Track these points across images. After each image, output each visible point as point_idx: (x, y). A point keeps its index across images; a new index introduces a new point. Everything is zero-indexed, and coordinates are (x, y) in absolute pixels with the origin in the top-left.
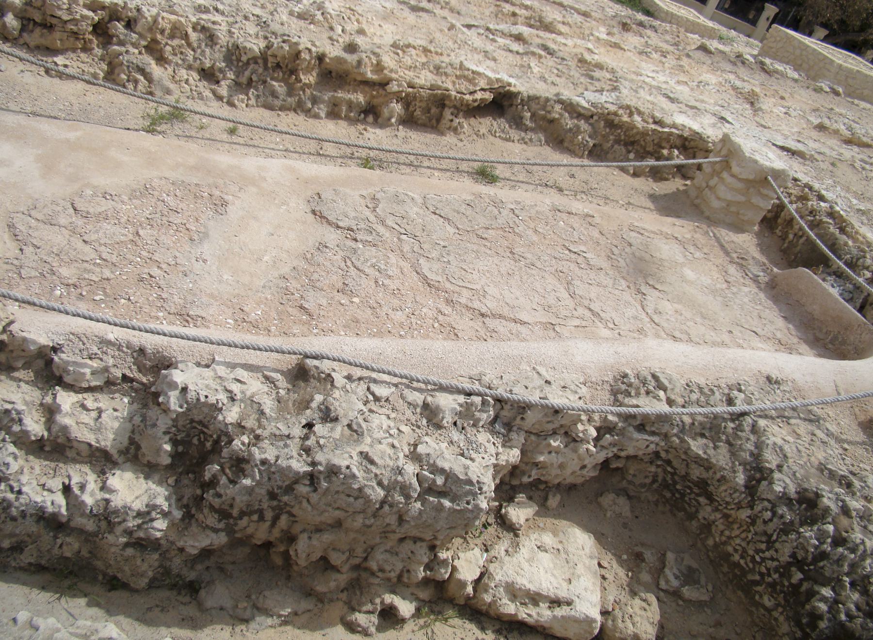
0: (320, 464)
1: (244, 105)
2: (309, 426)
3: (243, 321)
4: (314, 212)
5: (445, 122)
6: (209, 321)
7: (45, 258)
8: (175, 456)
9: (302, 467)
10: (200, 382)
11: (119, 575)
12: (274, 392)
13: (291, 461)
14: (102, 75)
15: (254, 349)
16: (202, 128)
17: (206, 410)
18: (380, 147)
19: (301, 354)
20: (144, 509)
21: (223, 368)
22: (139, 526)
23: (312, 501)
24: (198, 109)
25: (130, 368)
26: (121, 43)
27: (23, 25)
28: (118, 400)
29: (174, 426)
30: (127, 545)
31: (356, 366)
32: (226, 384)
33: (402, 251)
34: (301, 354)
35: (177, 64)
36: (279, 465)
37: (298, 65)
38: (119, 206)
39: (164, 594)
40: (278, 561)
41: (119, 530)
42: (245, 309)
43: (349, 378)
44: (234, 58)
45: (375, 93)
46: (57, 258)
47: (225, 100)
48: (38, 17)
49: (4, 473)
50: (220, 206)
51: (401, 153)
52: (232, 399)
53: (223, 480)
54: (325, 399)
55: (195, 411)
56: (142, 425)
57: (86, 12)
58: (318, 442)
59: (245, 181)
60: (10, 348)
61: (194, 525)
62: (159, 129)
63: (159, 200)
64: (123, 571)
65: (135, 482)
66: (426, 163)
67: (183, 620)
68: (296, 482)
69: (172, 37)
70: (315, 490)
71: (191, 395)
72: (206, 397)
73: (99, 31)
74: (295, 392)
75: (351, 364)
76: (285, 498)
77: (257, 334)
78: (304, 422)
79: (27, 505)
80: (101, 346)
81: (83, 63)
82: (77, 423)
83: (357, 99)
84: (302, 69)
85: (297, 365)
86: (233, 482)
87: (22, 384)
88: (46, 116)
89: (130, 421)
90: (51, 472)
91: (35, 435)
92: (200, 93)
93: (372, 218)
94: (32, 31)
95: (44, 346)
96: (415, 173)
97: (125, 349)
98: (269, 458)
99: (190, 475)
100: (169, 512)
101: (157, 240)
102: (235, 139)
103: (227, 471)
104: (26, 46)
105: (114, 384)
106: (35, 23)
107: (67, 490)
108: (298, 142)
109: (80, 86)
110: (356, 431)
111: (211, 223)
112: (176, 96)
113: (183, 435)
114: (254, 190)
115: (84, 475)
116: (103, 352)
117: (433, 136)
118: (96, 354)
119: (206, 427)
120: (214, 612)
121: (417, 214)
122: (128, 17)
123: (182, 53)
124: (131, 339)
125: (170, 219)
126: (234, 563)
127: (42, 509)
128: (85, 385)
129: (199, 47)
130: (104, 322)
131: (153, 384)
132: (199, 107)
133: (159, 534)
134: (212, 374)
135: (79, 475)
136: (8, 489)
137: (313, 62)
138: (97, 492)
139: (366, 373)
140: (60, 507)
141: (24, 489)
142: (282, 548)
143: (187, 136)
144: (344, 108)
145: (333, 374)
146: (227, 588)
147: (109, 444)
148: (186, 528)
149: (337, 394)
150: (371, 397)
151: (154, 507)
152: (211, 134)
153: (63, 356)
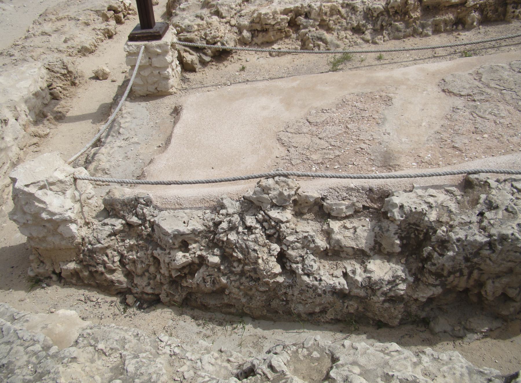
0: (494, 235)
1: (382, 41)
2: (481, 214)
3: (421, 162)
4: (444, 91)
5: (509, 15)
6: (403, 166)
7: (302, 152)
8: (402, 246)
9: (483, 239)
10: (409, 201)
11: (382, 319)
12: (454, 198)
13: (475, 236)
14: (299, 48)
15: (437, 175)
16: (362, 61)
17: (416, 216)
18: (471, 42)
19: (465, 173)
20: (391, 279)
21: (420, 190)
22: (390, 290)
23: (493, 259)
24: (355, 50)
25: (366, 201)
26: (305, 27)
27: (252, 34)
28: (363, 220)
29: (399, 229)
30: (384, 301)
31: (501, 173)
32: (424, 199)
33: (505, 100)
34: (465, 173)
35: (338, 30)
36: (469, 240)
37: (408, 8)
38: (332, 115)
39: (409, 327)
40: (475, 299)
41: (379, 293)
42: (421, 155)
43: (498, 181)
44: (369, 16)
45: (459, 11)
46: (308, 151)
47: (370, 42)
48: (259, 28)
49: (311, 271)
50: (388, 101)
51: (485, 42)
52: (431, 207)
53: (435, 255)
54: (487, 197)
55: (410, 218)
56: (380, 232)
57: (283, 17)
58: (489, 223)
59: (398, 83)
60: (300, 203)
61: (421, 284)
62: (338, 68)
63: (353, 106)
64: (384, 317)
65: (382, 265)
66: (504, 44)
67: (423, 341)
68: (481, 249)
69: (332, 15)
70: (494, 252)
71: (406, 209)
72: (416, 208)
73: (292, 25)
74: (467, 196)
75: (497, 173)
76: (475, 260)
77: (432, 168)
78: (477, 212)
79: (325, 286)
80: (347, 192)
81: (288, 44)
82: (344, 237)
83: (449, 17)
84: (411, 10)
85: (463, 180)
86: (442, 255)
87: (309, 221)
88: (277, 78)
89: (373, 231)
90: (335, 266)
91: (322, 248)
92: (355, 42)
93: (480, 85)
94: (257, 36)
95: (317, 198)
96: (498, 51)
97: (361, 191)
98: (461, 237)
99: (413, 256)
100: (406, 279)
101: (359, 128)
102: (382, 61)
103: (437, 249)
104: (256, 44)
105: (359, 212)
106: (258, 31)
107: (345, 275)
108: (421, 53)
109: (289, 57)
110: (511, 212)
111: (386, 112)
112: (343, 47)
113: (405, 233)
114: (405, 87)
115: (353, 265)
116: (349, 195)
117: (503, 26)
118: (346, 197)
119: (418, 226)
120: (440, 334)
121: (508, 75)
122: (305, 12)
123: (339, 22)
124: (364, 184)
125: (363, 115)
126: (447, 304)
127: (334, 288)
128: (343, 215)
129: (348, 16)
130: (348, 178)
131: (382, 207)
132: (357, 49)
133: (402, 293)
134: (414, 195)
135: (350, 266)
136: (314, 279)
137: (416, 4)
138: (363, 274)
139: (508, 176)
140: (344, 285)
141: (323, 278)
142: (476, 292)
143: (355, 68)
144: (442, 26)
145: (488, 181)
146: (446, 319)
147: (363, 246)
148: (417, 287)
149: (494, 192)
150: (515, 190)
151: (397, 277)
152: (368, 63)
153: (328, 201)
